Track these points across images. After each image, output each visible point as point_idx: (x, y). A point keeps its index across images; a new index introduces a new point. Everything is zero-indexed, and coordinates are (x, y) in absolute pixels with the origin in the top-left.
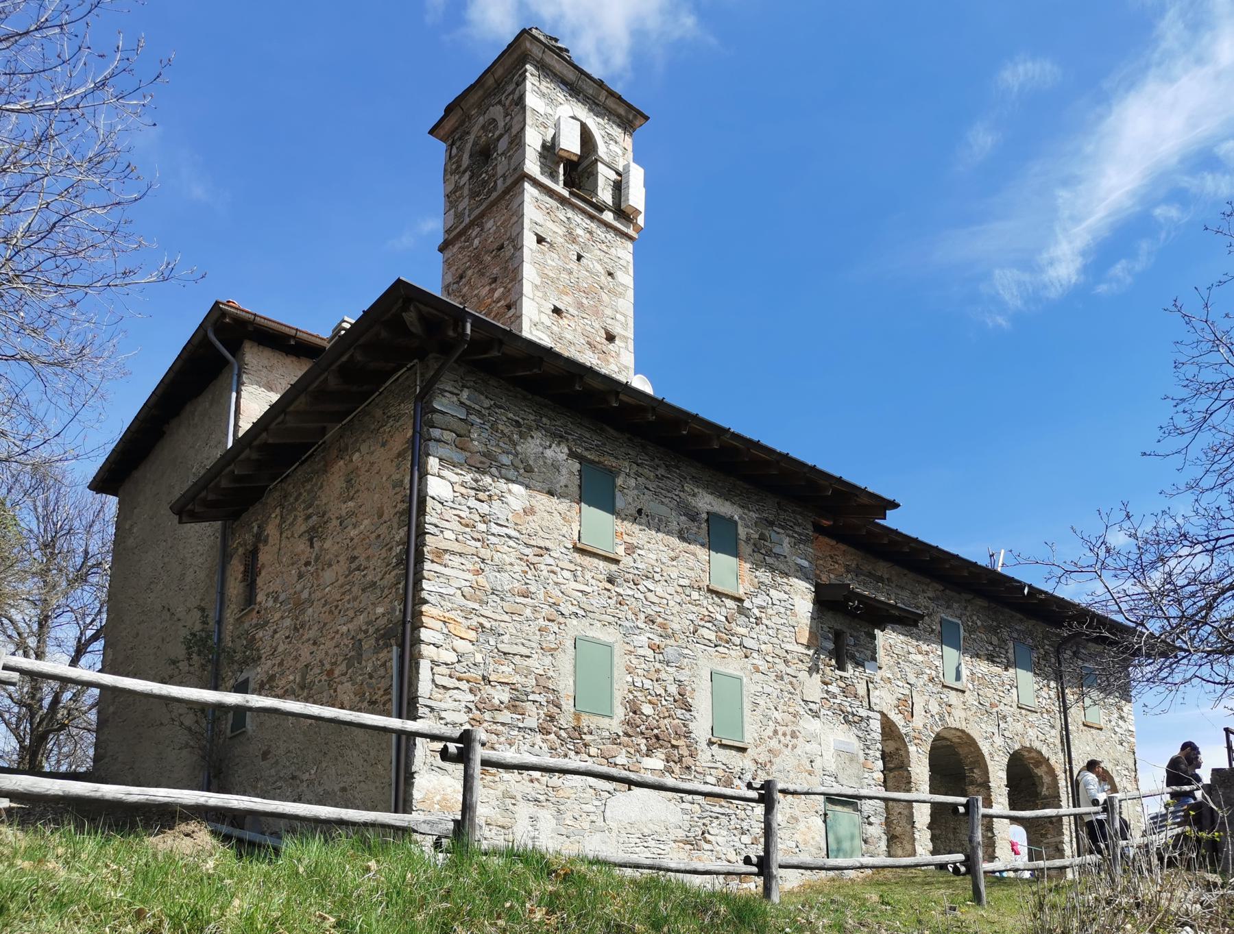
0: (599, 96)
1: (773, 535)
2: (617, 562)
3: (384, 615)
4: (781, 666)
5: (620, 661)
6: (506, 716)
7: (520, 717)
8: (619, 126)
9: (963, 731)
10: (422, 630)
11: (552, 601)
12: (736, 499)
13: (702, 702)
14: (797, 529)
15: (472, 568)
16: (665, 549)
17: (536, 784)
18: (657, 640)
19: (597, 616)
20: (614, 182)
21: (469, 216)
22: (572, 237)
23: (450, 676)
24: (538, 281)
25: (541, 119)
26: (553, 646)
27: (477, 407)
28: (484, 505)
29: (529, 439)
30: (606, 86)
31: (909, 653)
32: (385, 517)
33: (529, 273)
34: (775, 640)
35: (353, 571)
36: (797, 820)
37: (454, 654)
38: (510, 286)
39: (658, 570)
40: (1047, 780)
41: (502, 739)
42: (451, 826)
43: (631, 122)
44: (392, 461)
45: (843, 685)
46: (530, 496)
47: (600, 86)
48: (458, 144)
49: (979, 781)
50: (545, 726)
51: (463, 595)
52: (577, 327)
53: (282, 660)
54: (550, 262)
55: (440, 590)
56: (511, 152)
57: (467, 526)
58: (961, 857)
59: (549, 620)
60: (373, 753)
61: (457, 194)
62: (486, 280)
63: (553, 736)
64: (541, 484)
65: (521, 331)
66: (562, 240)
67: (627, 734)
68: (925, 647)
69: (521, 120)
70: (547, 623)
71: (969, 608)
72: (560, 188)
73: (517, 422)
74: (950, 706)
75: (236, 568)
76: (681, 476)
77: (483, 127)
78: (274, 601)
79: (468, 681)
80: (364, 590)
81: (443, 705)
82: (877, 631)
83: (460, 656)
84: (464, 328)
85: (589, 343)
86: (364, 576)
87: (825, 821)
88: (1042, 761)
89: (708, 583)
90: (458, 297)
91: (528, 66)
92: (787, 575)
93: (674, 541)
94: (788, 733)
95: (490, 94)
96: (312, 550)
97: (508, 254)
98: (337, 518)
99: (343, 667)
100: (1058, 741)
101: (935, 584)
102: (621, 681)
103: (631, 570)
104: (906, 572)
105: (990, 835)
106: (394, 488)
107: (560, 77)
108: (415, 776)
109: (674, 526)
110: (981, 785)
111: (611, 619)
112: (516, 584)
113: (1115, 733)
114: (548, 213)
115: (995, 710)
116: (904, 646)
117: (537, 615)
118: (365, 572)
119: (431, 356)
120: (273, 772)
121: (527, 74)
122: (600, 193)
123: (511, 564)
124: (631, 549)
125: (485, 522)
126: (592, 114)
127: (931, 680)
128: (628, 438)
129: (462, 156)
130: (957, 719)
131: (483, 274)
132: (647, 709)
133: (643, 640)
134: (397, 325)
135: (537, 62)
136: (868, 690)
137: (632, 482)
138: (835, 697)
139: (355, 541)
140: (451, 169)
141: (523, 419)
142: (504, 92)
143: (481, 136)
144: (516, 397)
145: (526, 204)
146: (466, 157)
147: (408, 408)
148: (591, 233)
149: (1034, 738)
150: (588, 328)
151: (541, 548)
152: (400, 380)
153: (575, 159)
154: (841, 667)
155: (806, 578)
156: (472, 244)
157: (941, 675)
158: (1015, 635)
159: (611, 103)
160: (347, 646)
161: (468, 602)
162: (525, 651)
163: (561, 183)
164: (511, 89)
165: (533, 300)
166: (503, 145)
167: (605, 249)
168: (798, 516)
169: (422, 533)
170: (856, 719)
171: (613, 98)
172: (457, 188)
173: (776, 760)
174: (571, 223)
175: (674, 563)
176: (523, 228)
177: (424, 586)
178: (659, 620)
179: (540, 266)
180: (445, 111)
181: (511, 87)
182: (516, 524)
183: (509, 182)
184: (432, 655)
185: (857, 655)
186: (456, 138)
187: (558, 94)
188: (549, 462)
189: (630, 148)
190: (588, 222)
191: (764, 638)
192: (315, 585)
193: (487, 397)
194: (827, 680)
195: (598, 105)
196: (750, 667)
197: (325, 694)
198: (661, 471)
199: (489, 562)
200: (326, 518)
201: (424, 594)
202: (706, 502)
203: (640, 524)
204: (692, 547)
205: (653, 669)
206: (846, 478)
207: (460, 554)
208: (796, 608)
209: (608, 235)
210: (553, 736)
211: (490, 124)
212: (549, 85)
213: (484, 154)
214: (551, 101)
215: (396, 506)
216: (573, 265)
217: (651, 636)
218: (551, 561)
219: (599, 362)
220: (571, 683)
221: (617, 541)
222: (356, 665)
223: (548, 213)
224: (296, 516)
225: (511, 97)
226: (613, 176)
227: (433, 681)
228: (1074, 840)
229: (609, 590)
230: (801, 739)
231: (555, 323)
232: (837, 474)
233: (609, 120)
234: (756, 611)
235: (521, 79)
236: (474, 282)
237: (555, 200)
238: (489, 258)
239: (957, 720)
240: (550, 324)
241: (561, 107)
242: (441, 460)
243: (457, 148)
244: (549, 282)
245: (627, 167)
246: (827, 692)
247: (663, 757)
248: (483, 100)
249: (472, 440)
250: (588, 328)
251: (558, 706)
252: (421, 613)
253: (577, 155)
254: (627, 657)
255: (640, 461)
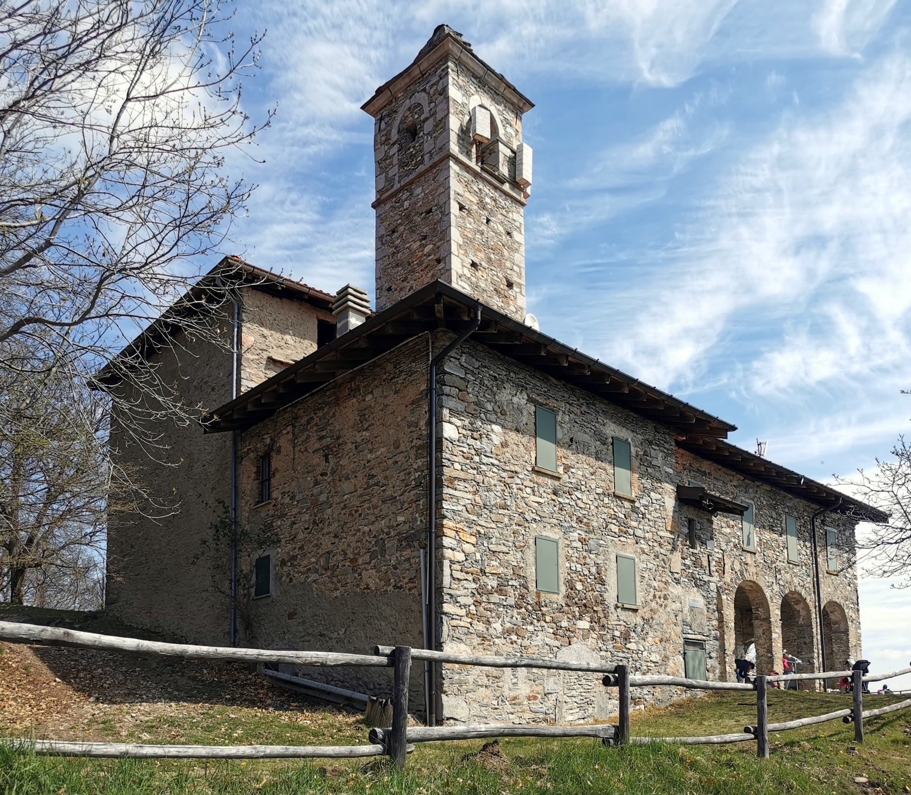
0: (499, 87)
1: (652, 451)
2: (559, 479)
3: (405, 522)
4: (657, 548)
5: (562, 553)
6: (495, 598)
7: (504, 597)
9: (754, 582)
10: (444, 538)
11: (520, 511)
12: (629, 425)
13: (611, 579)
14: (666, 445)
15: (471, 490)
16: (587, 467)
17: (515, 645)
18: (584, 535)
19: (547, 520)
22: (482, 205)
23: (461, 571)
26: (522, 544)
27: (471, 368)
28: (478, 442)
29: (503, 390)
31: (722, 527)
32: (402, 448)
33: (455, 235)
34: (653, 529)
35: (371, 486)
36: (669, 659)
37: (463, 555)
38: (439, 244)
39: (583, 483)
40: (803, 613)
41: (494, 614)
42: (613, 731)
44: (407, 406)
45: (694, 559)
46: (505, 433)
48: (387, 119)
49: (763, 617)
50: (519, 603)
51: (467, 511)
53: (303, 545)
54: (468, 225)
55: (455, 508)
56: (436, 134)
57: (467, 458)
58: (847, 711)
59: (519, 525)
60: (401, 626)
61: (388, 162)
62: (415, 237)
63: (523, 609)
64: (511, 424)
65: (450, 282)
66: (476, 207)
67: (567, 605)
68: (732, 523)
70: (518, 527)
71: (759, 492)
72: (473, 164)
73: (495, 377)
74: (747, 564)
75: (248, 469)
76: (596, 411)
77: (409, 109)
78: (291, 499)
79: (472, 574)
80: (384, 502)
81: (458, 593)
82: (713, 518)
83: (467, 555)
85: (495, 290)
86: (383, 491)
87: (684, 659)
88: (801, 600)
89: (613, 490)
90: (391, 247)
92: (660, 481)
93: (592, 460)
94: (662, 596)
96: (327, 464)
97: (437, 218)
98: (353, 443)
99: (367, 557)
100: (811, 586)
101: (738, 476)
102: (564, 565)
103: (568, 484)
104: (721, 467)
105: (769, 655)
106: (409, 427)
108: (443, 645)
109: (593, 450)
110: (764, 620)
111: (556, 522)
112: (499, 500)
113: (846, 577)
115: (774, 565)
116: (719, 522)
117: (512, 522)
118: (384, 488)
119: (440, 329)
120: (301, 628)
123: (495, 485)
124: (567, 468)
125: (478, 455)
127: (735, 546)
128: (564, 385)
129: (390, 130)
130: (751, 574)
131: (414, 232)
132: (579, 586)
133: (575, 535)
134: (428, 309)
136: (709, 562)
137: (567, 418)
138: (689, 568)
139: (373, 462)
141: (499, 375)
142: (428, 83)
144: (494, 358)
145: (451, 178)
146: (394, 132)
147: (421, 367)
148: (495, 201)
149: (797, 584)
150: (495, 278)
151: (512, 472)
152: (410, 344)
154: (693, 547)
155: (672, 482)
157: (741, 542)
158: (787, 510)
159: (508, 93)
160: (370, 542)
161: (470, 516)
162: (505, 549)
163: (474, 160)
164: (435, 81)
166: (428, 126)
167: (505, 213)
168: (667, 437)
169: (440, 466)
170: (702, 583)
172: (387, 157)
173: (656, 616)
174: (482, 193)
175: (593, 477)
176: (449, 198)
177: (444, 506)
178: (585, 520)
179: (462, 228)
181: (434, 80)
182: (497, 455)
183: (436, 159)
184: (450, 556)
185: (702, 536)
186: (384, 114)
188: (516, 406)
189: (520, 130)
190: (493, 192)
191: (647, 528)
192: (332, 492)
193: (477, 360)
194: (684, 556)
195: (498, 94)
196: (639, 550)
197: (349, 576)
198: (584, 408)
199: (481, 484)
200: (340, 441)
201: (444, 512)
202: (612, 429)
203: (572, 449)
204: (603, 464)
205: (582, 556)
206: (706, 411)
207: (465, 480)
208: (666, 505)
210: (523, 609)
211: (416, 107)
213: (412, 132)
214: (467, 94)
215: (412, 442)
216: (484, 228)
217: (580, 532)
218: (519, 481)
219: (503, 305)
220: (534, 570)
221: (559, 463)
222: (379, 557)
224: (308, 437)
225: (435, 87)
227: (451, 575)
228: (821, 656)
229: (554, 500)
230: (669, 600)
232: (701, 409)
233: (505, 107)
234: (642, 509)
235: (444, 73)
237: (471, 174)
239: (751, 574)
240: (469, 276)
242: (450, 410)
243: (386, 124)
245: (520, 147)
246: (685, 565)
247: (589, 619)
249: (468, 393)
250: (495, 278)
251: (527, 588)
252: (442, 526)
253: (488, 139)
254: (566, 549)
255: (571, 402)
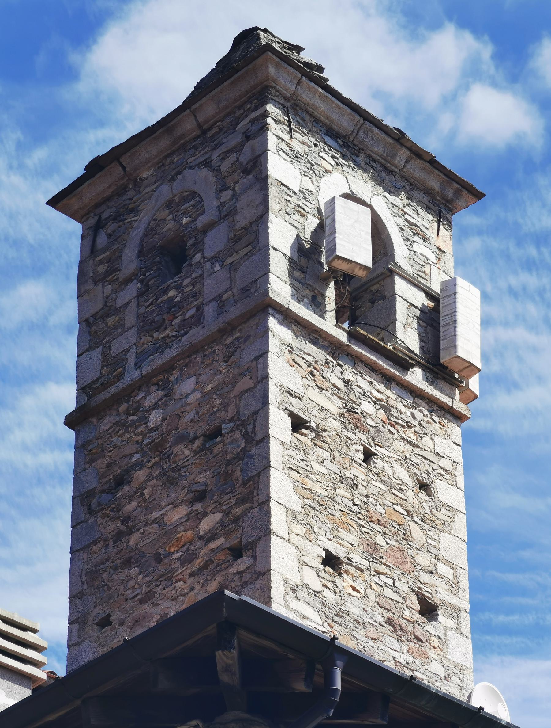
8: (428, 209)
20: (421, 311)
21: (138, 366)
24: (296, 504)
25: (294, 200)
30: (408, 140)
43: (450, 201)
47: (398, 140)
48: (111, 227)
52: (369, 591)
54: (316, 467)
56: (235, 257)
61: (111, 321)
65: (268, 602)
66: (337, 424)
69: (259, 201)
84: (329, 678)
85: (390, 622)
90: (113, 519)
91: (270, 107)
95: (184, 145)
97: (233, 450)
107: (324, 124)
114: (311, 373)
119: (231, 715)
121: (269, 120)
122: (400, 334)
126: (381, 189)
135: (286, 98)
140: (95, 271)
143: (163, 220)
145: (272, 359)
148: (386, 408)
150: (388, 592)
153: (361, 273)
156: (144, 420)
165: (289, 541)
171: (419, 162)
174: (351, 390)
180: (87, 168)
181: (233, 140)
183: (233, 313)
186: (105, 215)
187: (323, 154)
190: (382, 388)
195: (390, 172)
209: (416, 412)
211: (185, 200)
212: (305, 139)
219: (410, 659)
223: (311, 373)
225: (233, 157)
226: (420, 299)
231: (329, 585)
235: (254, 128)
236: (151, 495)
237: (322, 348)
238: (187, 452)
240: (318, 587)
241: (327, 177)
244: (316, 505)
248: (170, 155)
253: (366, 268)
